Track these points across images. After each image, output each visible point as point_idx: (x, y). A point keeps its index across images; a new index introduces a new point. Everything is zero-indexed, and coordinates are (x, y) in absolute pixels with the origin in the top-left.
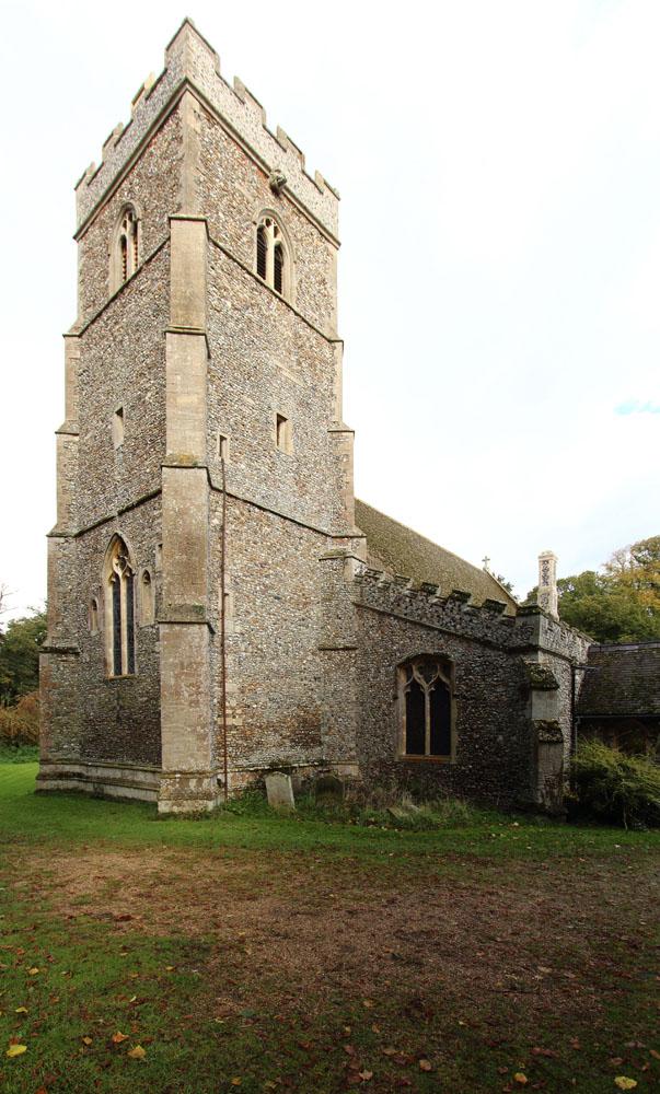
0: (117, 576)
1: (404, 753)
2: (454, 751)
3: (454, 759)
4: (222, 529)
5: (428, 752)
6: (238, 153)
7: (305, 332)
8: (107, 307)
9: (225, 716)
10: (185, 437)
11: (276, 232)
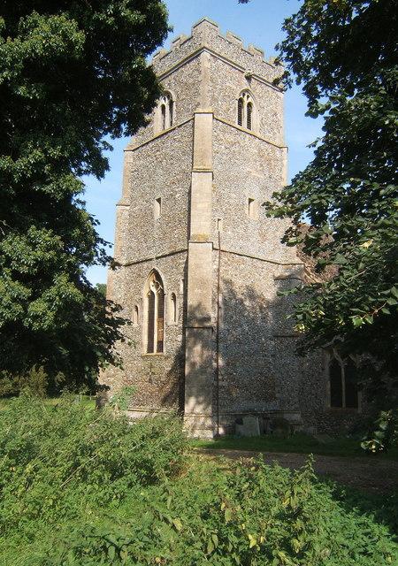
0: (152, 293)
1: (329, 406)
2: (360, 405)
3: (360, 411)
4: (219, 270)
5: (344, 406)
6: (228, 67)
7: (264, 146)
8: (153, 140)
9: (217, 380)
10: (201, 223)
11: (248, 97)
